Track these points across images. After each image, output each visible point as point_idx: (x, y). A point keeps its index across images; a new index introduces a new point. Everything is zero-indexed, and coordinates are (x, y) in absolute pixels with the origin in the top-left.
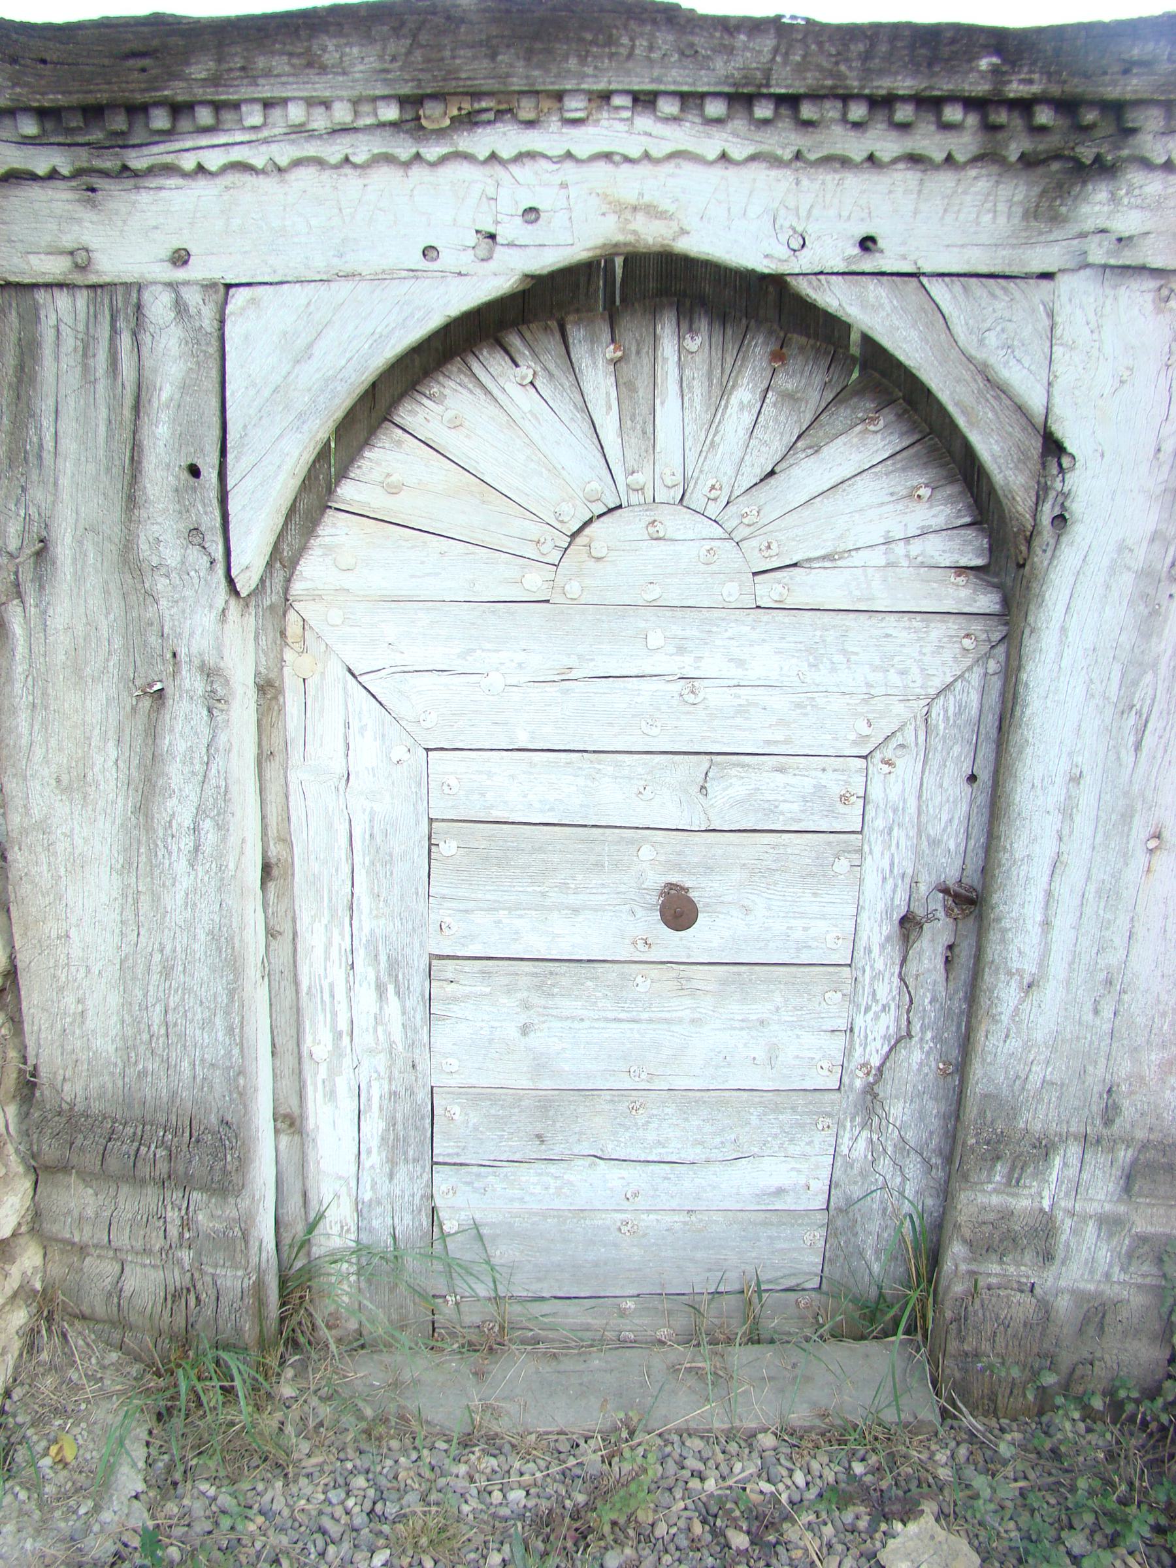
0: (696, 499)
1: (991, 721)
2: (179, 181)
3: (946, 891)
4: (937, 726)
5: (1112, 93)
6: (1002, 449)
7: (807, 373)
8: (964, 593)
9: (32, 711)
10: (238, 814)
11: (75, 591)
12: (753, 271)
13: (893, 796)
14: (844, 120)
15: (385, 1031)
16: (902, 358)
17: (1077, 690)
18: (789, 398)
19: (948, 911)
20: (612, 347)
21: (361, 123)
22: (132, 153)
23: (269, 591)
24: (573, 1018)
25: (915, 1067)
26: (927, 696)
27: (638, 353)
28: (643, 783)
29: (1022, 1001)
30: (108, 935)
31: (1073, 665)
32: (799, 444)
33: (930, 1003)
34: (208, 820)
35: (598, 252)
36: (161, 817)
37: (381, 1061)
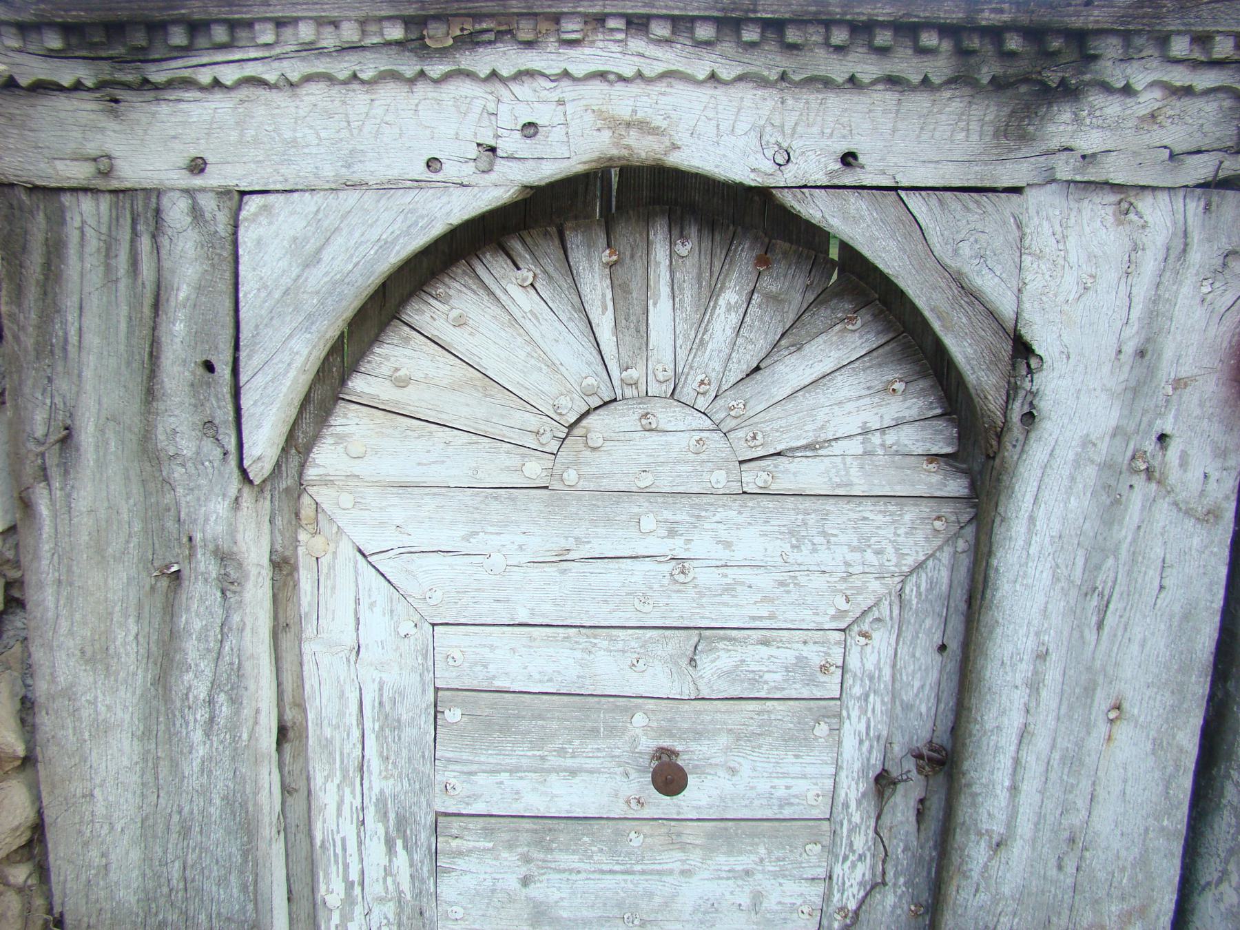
0: (687, 393)
1: (960, 595)
2: (198, 95)
3: (919, 756)
4: (910, 601)
5: (1077, 22)
6: (975, 351)
7: (789, 277)
8: (935, 479)
9: (58, 586)
10: (252, 687)
11: (98, 476)
12: (741, 184)
13: (870, 666)
14: (827, 44)
15: (394, 881)
16: (881, 266)
17: (1045, 574)
18: (774, 299)
19: (920, 770)
20: (608, 251)
21: (368, 42)
22: (152, 68)
23: (285, 474)
24: (571, 871)
25: (889, 909)
26: (901, 573)
27: (632, 257)
28: (636, 656)
29: (990, 859)
30: (130, 796)
31: (1040, 552)
32: (783, 342)
33: (903, 852)
34: (222, 694)
35: (594, 165)
36: (178, 690)
37: (390, 909)
